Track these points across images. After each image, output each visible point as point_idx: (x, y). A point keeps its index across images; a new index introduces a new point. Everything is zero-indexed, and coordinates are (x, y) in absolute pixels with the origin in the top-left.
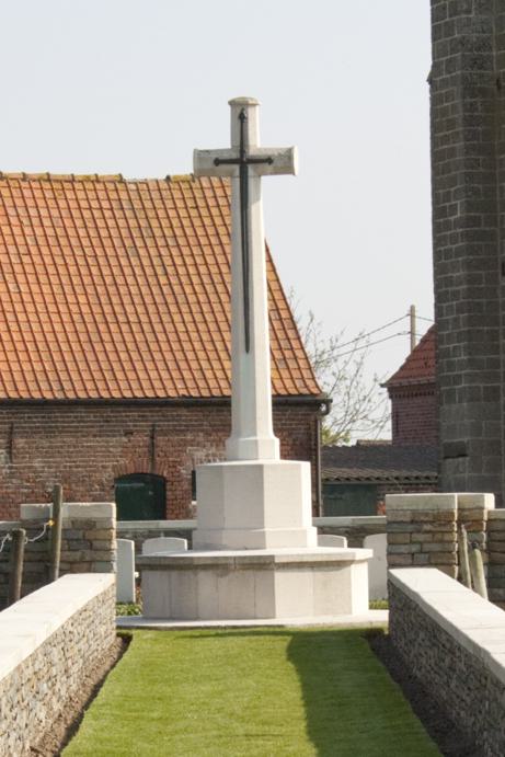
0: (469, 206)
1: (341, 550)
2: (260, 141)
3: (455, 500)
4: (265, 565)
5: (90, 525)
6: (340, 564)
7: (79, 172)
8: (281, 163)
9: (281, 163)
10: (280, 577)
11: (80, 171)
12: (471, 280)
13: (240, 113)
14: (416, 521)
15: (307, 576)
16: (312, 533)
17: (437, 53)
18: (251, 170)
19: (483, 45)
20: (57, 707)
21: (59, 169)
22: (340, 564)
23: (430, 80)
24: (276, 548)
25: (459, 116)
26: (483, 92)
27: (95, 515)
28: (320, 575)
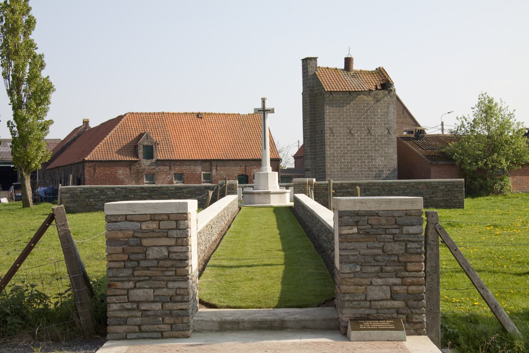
0: (310, 120)
2: (267, 107)
3: (307, 180)
5: (233, 185)
6: (284, 193)
7: (231, 113)
8: (272, 111)
9: (272, 111)
10: (271, 196)
12: (311, 135)
18: (266, 112)
19: (313, 87)
22: (284, 193)
23: (302, 94)
24: (271, 190)
25: (308, 101)
26: (313, 96)
27: (234, 183)
28: (280, 195)
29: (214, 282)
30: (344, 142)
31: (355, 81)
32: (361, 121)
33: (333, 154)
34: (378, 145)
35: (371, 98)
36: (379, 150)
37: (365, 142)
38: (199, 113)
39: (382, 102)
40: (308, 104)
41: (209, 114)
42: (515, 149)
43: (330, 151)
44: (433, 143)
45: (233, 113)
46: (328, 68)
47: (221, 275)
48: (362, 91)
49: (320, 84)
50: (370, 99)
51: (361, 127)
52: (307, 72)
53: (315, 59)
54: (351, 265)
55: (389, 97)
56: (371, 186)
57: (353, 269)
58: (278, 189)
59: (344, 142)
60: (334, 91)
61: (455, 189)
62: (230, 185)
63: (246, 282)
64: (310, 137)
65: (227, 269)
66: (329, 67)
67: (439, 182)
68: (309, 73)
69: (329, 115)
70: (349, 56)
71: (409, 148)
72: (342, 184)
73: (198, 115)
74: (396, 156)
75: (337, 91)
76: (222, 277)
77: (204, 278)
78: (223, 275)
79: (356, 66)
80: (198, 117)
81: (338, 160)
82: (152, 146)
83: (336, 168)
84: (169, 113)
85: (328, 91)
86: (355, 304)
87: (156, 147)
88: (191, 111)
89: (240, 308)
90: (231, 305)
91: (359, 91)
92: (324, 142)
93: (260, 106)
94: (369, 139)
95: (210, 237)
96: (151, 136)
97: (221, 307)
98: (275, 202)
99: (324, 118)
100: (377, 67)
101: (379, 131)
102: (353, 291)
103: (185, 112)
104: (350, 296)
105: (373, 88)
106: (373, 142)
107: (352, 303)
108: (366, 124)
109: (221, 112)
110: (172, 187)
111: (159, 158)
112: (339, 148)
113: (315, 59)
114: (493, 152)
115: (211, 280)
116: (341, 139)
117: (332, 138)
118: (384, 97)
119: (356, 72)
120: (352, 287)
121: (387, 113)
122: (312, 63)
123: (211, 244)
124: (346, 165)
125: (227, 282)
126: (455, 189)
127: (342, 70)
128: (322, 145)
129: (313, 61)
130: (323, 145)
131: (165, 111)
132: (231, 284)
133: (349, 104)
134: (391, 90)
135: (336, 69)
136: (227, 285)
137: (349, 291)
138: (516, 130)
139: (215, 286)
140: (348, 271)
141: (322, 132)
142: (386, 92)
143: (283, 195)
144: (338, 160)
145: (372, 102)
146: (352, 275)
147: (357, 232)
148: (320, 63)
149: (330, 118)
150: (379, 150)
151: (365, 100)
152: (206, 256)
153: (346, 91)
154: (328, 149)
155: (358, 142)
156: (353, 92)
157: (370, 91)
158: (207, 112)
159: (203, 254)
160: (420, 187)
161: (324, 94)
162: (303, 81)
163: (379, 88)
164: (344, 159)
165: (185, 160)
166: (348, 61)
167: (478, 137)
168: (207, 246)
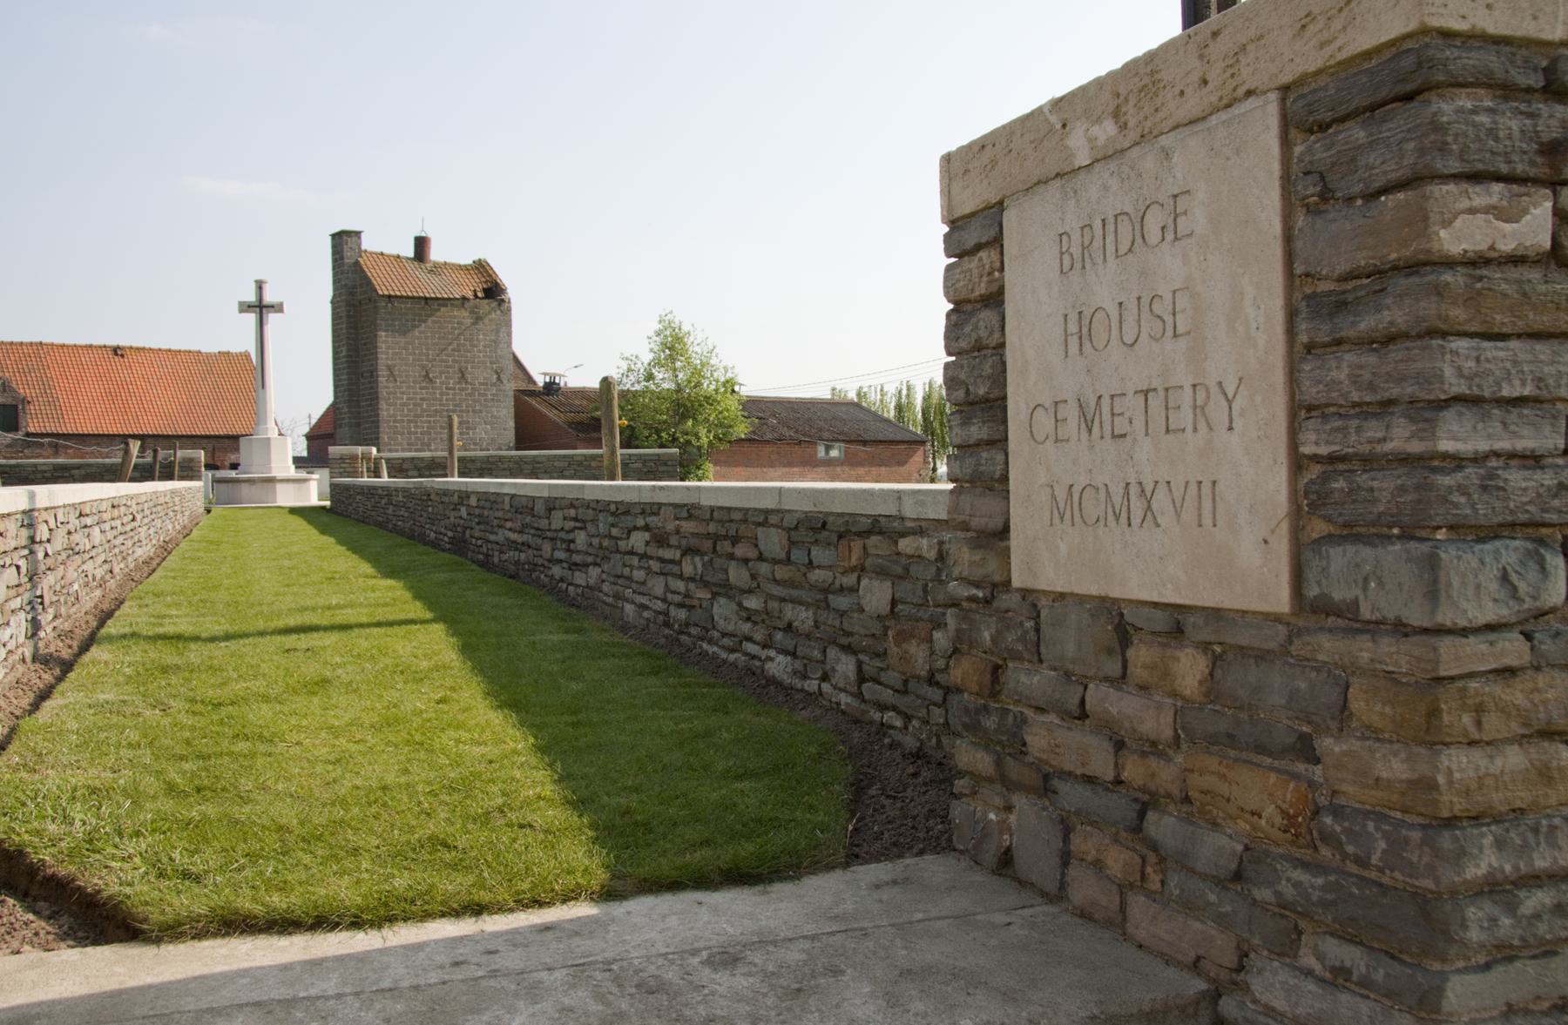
0: (348, 350)
1: (303, 474)
2: (269, 298)
3: (359, 450)
4: (272, 480)
5: (191, 460)
6: (305, 480)
7: (183, 348)
8: (278, 308)
9: (278, 308)
10: (279, 487)
11: (183, 348)
12: (349, 379)
13: (260, 286)
14: (342, 458)
15: (291, 486)
16: (293, 467)
17: (335, 290)
18: (264, 310)
19: (354, 287)
20: (178, 527)
21: (175, 347)
22: (305, 480)
23: (332, 302)
24: (277, 472)
25: (344, 314)
26: (354, 306)
27: (193, 456)
28: (296, 486)
29: (128, 710)
30: (415, 393)
31: (436, 280)
32: (448, 355)
33: (394, 416)
34: (479, 401)
35: (466, 314)
36: (481, 411)
37: (454, 394)
38: (118, 347)
39: (486, 321)
40: (344, 319)
41: (138, 349)
42: (721, 413)
43: (388, 410)
44: (577, 402)
45: (187, 348)
46: (382, 254)
47: (165, 670)
48: (449, 299)
49: (369, 282)
50: (463, 315)
51: (447, 367)
52: (342, 258)
53: (358, 234)
54: (1510, 552)
55: (498, 312)
56: (493, 463)
57: (1522, 587)
58: (291, 472)
59: (415, 393)
60: (396, 296)
61: (661, 468)
62: (184, 459)
63: (300, 702)
64: (349, 385)
65: (364, 620)
66: (385, 252)
67: (630, 455)
68: (346, 261)
69: (386, 342)
70: (423, 234)
71: (535, 409)
72: (433, 459)
73: (116, 350)
74: (512, 424)
75: (402, 297)
76: (174, 680)
77: (81, 687)
78: (178, 667)
79: (436, 254)
80: (116, 354)
81: (403, 427)
82: (16, 407)
83: (401, 444)
84: (52, 345)
85: (383, 296)
86: (1537, 916)
87: (23, 409)
88: (101, 343)
89: (321, 922)
90: (246, 903)
91: (443, 299)
92: (377, 393)
93: (251, 297)
94: (462, 389)
95: (129, 543)
96: (14, 386)
97: (173, 931)
98: (287, 497)
99: (376, 347)
100: (476, 258)
101: (480, 375)
102: (1522, 797)
103: (88, 343)
104: (1500, 844)
105: (470, 295)
106: (470, 395)
107: (1512, 908)
108: (456, 361)
109: (164, 347)
110: (45, 464)
111: (31, 430)
112: (404, 405)
113: (358, 234)
114: (684, 418)
115: (109, 696)
116: (409, 387)
117: (391, 385)
118: (490, 313)
119: (436, 265)
120: (1514, 759)
121: (495, 342)
122: (351, 241)
123: (132, 566)
124: (418, 439)
125: (199, 707)
126: (661, 468)
127: (408, 258)
128: (372, 400)
129: (354, 239)
130: (374, 398)
131: (46, 340)
132: (224, 711)
133: (425, 321)
134: (503, 300)
135: (398, 257)
136: (200, 722)
137: (1497, 800)
138: (722, 379)
139: (134, 736)
140: (1489, 613)
141: (373, 373)
142: (494, 304)
143: (304, 485)
144: (403, 427)
145: (468, 321)
146: (1513, 649)
147: (1546, 243)
148: (367, 244)
149: (388, 348)
150: (481, 411)
151: (455, 317)
152: (107, 600)
153: (420, 298)
154: (385, 407)
155: (441, 394)
156: (432, 299)
157: (464, 299)
158: (135, 345)
159: (98, 593)
160: (593, 464)
161: (375, 302)
162: (335, 275)
163: (480, 295)
164: (416, 427)
165: (89, 435)
166: (421, 244)
167: (659, 396)
168: (116, 570)
